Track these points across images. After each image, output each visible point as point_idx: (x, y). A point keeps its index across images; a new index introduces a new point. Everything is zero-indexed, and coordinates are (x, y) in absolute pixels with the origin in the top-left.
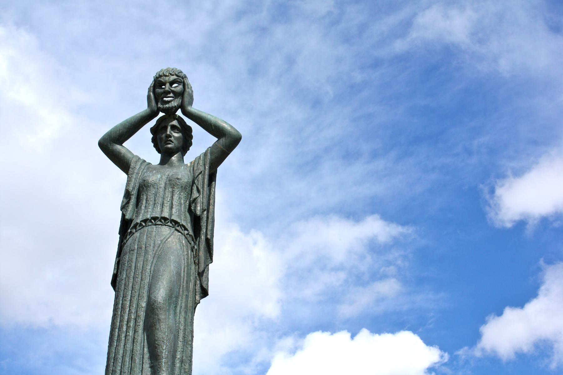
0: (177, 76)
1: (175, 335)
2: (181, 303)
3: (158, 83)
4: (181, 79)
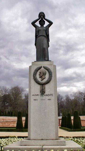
4: (43, 14)
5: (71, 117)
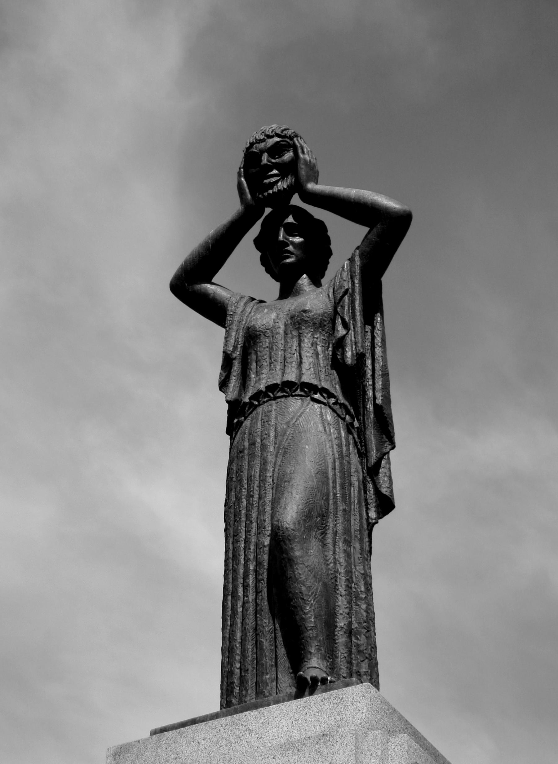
0: (278, 135)
1: (325, 585)
2: (337, 524)
3: (251, 158)
4: (286, 143)
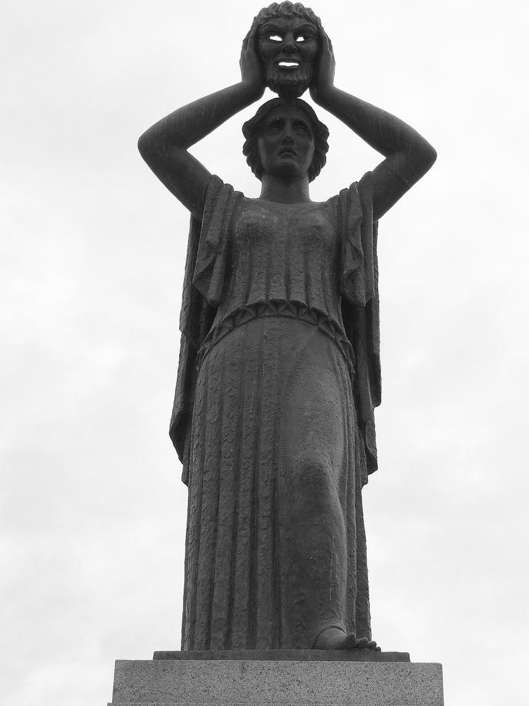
5: (385, 158)
